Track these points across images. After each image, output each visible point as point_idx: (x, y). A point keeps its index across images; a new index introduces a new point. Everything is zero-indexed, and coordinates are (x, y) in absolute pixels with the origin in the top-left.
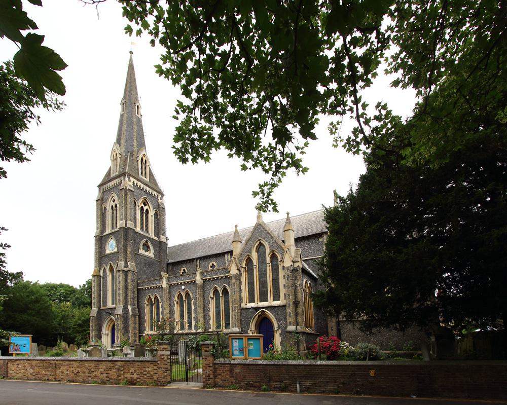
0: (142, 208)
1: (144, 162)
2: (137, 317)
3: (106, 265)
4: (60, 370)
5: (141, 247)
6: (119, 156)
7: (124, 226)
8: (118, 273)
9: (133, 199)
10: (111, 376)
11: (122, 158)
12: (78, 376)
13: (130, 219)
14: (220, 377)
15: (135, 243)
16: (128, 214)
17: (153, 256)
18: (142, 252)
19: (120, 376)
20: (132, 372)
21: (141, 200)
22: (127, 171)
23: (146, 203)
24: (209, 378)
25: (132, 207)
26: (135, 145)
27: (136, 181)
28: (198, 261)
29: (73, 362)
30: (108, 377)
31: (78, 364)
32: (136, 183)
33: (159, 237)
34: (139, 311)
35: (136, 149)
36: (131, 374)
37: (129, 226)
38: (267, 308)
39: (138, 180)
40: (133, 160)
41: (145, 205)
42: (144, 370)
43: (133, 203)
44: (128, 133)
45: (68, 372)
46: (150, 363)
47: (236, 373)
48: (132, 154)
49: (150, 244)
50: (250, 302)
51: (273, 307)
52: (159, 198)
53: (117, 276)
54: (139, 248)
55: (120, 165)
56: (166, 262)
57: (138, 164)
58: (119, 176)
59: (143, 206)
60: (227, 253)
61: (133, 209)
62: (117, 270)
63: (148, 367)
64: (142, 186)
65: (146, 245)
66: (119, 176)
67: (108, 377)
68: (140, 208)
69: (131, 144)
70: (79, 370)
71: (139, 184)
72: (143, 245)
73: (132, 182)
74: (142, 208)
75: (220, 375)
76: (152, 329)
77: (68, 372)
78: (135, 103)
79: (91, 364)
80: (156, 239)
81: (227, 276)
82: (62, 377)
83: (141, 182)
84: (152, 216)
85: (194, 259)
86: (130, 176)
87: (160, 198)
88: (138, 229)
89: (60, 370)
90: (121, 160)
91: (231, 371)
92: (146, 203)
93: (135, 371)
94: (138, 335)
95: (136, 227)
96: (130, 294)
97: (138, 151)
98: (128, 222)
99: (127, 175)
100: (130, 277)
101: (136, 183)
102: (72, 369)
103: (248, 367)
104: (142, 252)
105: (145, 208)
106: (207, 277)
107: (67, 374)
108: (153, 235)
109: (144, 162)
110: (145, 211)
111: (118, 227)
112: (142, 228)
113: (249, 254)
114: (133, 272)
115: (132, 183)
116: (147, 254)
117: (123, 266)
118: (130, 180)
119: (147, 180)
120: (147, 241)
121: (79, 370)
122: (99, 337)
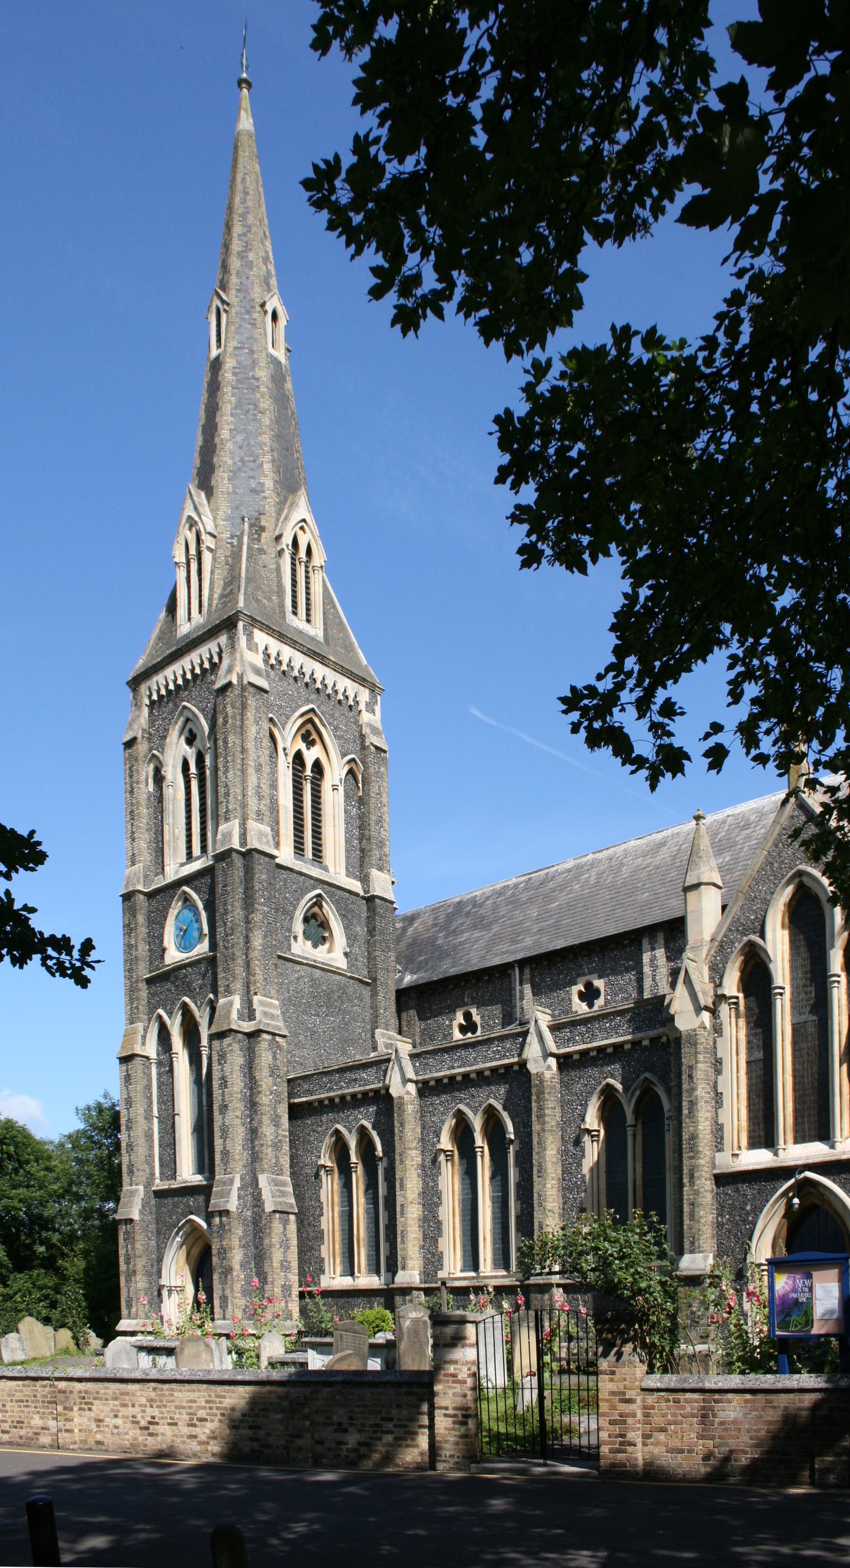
0: (299, 758)
1: (302, 553)
2: (292, 1218)
3: (170, 1014)
4: (92, 1414)
5: (298, 927)
6: (208, 541)
7: (236, 844)
8: (216, 1044)
9: (266, 725)
10: (269, 1434)
11: (220, 552)
12: (151, 1435)
13: (259, 813)
14: (662, 1437)
15: (277, 910)
16: (251, 792)
17: (341, 963)
18: (301, 948)
19: (300, 1436)
20: (340, 1424)
21: (294, 724)
22: (241, 604)
23: (315, 736)
24: (621, 1444)
25: (265, 759)
26: (269, 483)
27: (275, 646)
28: (527, 971)
29: (136, 1387)
30: (256, 1440)
31: (153, 1395)
32: (273, 655)
33: (365, 879)
34: (297, 1196)
35: (270, 509)
36: (336, 1431)
37: (254, 843)
38: (823, 1168)
39: (281, 637)
40: (262, 551)
41: (310, 744)
42: (384, 1415)
43: (266, 742)
44: (239, 438)
45: (119, 1421)
46: (405, 1389)
47: (722, 1423)
48: (258, 529)
49: (330, 911)
50: (753, 1144)
51: (174, 1132)
52: (362, 706)
53: (215, 1058)
54: (289, 937)
55: (212, 583)
56: (393, 988)
57: (278, 569)
58: (211, 633)
59: (302, 746)
60: (650, 932)
61: (266, 769)
62: (214, 1030)
63: (399, 1406)
64: (299, 659)
65: (314, 916)
66: (211, 633)
67: (256, 1440)
68: (290, 759)
69: (253, 484)
70: (156, 1412)
71: (287, 652)
72: (306, 920)
73: (261, 648)
74: (299, 758)
75: (663, 1430)
76: (350, 1270)
77: (119, 1421)
78: (263, 305)
79: (196, 1394)
80: (356, 886)
81: (659, 1037)
82: (99, 1437)
83: (293, 644)
84: (335, 788)
85: (509, 966)
86: (254, 622)
87: (368, 704)
88: (285, 855)
89: (92, 1414)
90: (214, 559)
91: (705, 1416)
92: (315, 736)
93: (351, 1418)
94: (295, 1291)
95: (277, 845)
96: (239, 1134)
97: (279, 512)
98: (252, 824)
99: (240, 625)
100: (265, 1057)
101: (273, 655)
102: (130, 1411)
103: (768, 1401)
104: (301, 948)
105: (311, 756)
106: (575, 1042)
107: (116, 1427)
108: (343, 871)
109: (302, 553)
110: (308, 772)
111: (210, 852)
112: (299, 848)
113: (756, 938)
114: (274, 1034)
115: (261, 656)
116: (320, 954)
117: (234, 1015)
118: (252, 646)
119: (316, 630)
120: (318, 902)
121: (156, 1412)
122: (157, 1295)
